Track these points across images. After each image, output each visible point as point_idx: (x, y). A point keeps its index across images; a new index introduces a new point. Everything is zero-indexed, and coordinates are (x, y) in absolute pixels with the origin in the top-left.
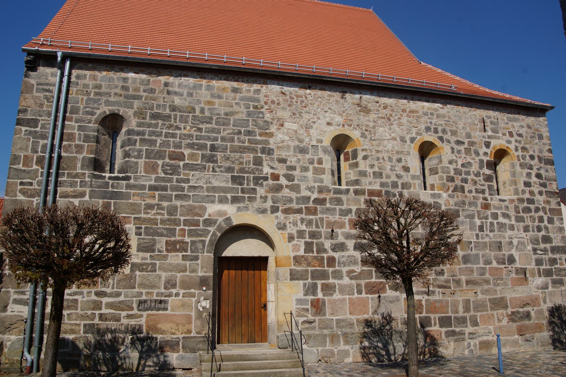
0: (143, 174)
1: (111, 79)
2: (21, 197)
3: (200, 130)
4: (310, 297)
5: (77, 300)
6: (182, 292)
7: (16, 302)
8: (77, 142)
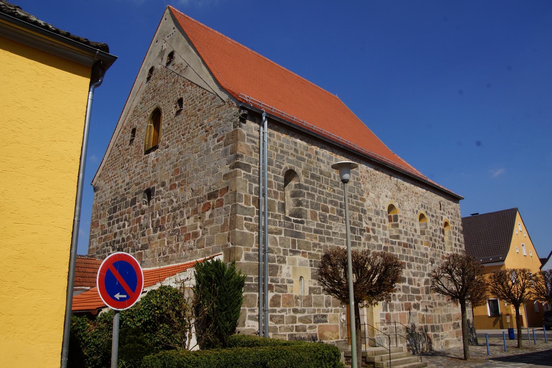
0: (310, 220)
1: (288, 142)
2: (246, 230)
3: (334, 191)
4: (385, 312)
5: (283, 316)
6: (334, 308)
7: (251, 318)
8: (274, 189)
